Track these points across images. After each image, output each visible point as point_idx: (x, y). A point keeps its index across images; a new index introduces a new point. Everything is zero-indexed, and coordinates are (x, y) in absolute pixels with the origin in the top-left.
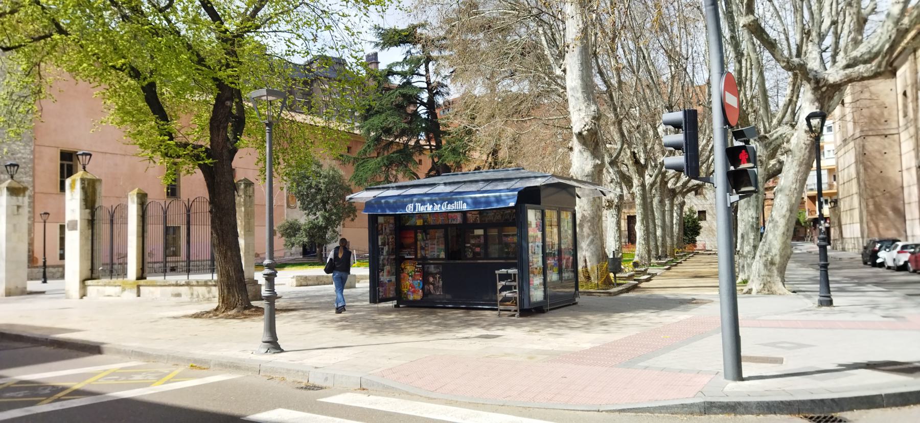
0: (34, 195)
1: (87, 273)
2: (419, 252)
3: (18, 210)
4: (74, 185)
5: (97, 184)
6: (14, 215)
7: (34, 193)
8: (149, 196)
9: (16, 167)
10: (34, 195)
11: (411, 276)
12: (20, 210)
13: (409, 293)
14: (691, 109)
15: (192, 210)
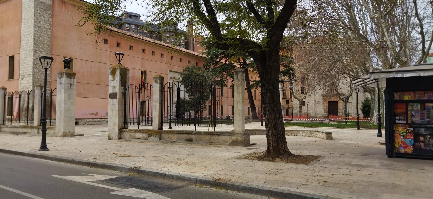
0: (51, 81)
1: (122, 125)
2: (409, 118)
3: (71, 87)
5: (127, 71)
6: (69, 89)
7: (51, 80)
8: (7, 90)
9: (121, 56)
10: (51, 81)
11: (403, 136)
12: (72, 86)
13: (401, 148)
15: (22, 96)
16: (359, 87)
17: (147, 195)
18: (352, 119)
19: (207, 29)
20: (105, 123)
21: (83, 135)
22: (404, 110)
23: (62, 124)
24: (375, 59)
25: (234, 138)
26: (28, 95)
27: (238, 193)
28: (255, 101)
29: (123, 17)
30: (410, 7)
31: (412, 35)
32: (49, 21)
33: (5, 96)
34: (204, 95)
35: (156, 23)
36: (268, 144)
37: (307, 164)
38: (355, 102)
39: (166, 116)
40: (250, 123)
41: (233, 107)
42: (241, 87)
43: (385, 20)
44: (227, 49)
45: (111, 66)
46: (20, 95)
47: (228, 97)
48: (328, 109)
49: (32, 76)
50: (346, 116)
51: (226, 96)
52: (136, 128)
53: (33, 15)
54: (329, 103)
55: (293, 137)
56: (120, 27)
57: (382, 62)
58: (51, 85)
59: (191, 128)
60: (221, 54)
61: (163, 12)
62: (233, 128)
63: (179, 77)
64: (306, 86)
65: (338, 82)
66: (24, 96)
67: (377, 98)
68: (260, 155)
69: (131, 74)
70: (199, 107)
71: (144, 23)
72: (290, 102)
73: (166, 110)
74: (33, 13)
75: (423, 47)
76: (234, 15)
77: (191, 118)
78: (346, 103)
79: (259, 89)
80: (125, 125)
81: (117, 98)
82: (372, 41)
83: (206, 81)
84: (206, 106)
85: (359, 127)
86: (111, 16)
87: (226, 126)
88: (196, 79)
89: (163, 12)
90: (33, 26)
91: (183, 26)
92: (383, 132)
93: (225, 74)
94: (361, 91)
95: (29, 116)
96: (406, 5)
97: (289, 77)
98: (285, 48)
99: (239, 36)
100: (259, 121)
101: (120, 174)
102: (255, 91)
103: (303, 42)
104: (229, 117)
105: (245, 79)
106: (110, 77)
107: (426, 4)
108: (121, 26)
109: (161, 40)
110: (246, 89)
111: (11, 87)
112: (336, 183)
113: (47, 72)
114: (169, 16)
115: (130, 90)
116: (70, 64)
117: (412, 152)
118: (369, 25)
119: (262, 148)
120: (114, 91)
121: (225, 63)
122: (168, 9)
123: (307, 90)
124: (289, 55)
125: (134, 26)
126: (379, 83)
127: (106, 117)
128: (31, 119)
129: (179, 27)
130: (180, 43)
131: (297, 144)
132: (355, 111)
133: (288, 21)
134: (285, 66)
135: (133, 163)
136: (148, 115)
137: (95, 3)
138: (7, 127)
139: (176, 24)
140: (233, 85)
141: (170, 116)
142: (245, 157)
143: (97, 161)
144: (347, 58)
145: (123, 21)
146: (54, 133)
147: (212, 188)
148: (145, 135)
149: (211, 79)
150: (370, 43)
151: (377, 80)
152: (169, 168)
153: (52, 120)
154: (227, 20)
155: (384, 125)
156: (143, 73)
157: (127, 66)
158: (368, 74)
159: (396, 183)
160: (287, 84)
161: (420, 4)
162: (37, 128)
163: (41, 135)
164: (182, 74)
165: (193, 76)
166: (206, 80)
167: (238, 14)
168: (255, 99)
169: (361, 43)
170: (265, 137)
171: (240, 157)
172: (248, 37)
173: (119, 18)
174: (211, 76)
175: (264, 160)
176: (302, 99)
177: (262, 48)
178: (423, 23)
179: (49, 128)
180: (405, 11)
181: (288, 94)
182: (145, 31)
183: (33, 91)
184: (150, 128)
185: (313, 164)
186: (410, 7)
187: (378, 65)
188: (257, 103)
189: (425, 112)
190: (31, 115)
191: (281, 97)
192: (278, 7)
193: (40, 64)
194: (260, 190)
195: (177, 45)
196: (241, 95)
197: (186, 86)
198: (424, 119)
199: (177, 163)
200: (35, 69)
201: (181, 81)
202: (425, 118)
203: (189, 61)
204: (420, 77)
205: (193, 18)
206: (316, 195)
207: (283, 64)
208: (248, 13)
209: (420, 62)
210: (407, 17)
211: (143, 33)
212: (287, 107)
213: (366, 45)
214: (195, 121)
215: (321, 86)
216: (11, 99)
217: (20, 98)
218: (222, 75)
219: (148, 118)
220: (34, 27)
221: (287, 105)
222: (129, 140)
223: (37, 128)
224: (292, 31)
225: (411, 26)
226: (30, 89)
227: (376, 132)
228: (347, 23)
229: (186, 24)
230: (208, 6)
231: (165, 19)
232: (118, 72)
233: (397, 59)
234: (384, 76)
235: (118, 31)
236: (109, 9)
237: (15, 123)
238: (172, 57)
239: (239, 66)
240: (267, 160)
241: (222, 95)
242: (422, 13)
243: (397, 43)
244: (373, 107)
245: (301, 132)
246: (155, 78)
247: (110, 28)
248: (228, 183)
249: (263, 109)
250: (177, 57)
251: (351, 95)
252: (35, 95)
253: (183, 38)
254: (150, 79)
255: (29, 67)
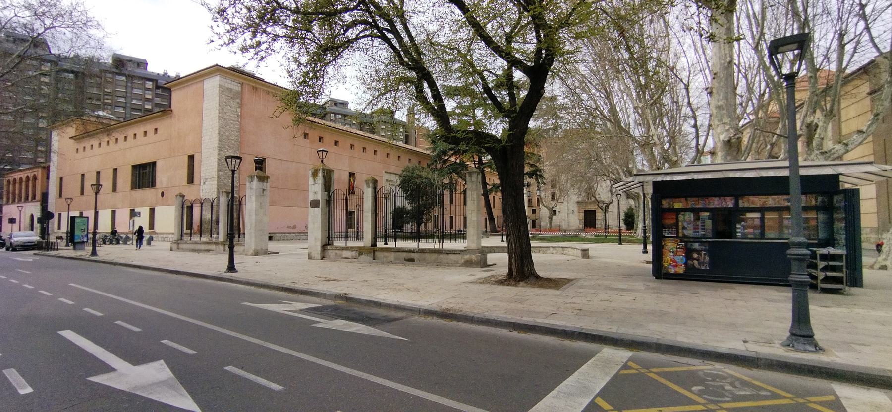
1: (325, 241)
2: (680, 231)
4: (317, 174)
14: (434, 76)
15: (204, 205)
16: (621, 192)
17: (358, 328)
18: (613, 232)
19: (432, 119)
20: (305, 238)
21: (278, 253)
22: (674, 221)
23: (253, 239)
24: (639, 158)
25: (467, 257)
26: (212, 203)
27: (472, 326)
28: (493, 210)
29: (327, 105)
30: (681, 95)
31: (683, 129)
32: (237, 111)
33: (183, 205)
34: (429, 203)
35: (368, 112)
36: (510, 264)
37: (558, 289)
38: (616, 211)
39: (381, 230)
40: (487, 237)
41: (466, 218)
42: (475, 192)
43: (651, 110)
44: (458, 144)
45: (312, 166)
46: (202, 204)
47: (460, 204)
48: (585, 219)
49: (216, 179)
50: (605, 229)
51: (457, 204)
52: (343, 244)
53: (217, 105)
54: (586, 213)
55: (541, 255)
56: (323, 117)
57: (648, 161)
58: (239, 190)
59: (412, 245)
60: (450, 149)
61: (377, 98)
62: (465, 245)
63: (398, 180)
64: (557, 191)
65: (595, 186)
66: (207, 205)
67: (642, 206)
68: (500, 278)
69: (336, 177)
70: (422, 218)
71: (353, 113)
72: (537, 211)
73: (381, 221)
74: (218, 101)
75: (697, 144)
76: (467, 101)
77: (411, 232)
78: (605, 213)
79: (499, 195)
80: (329, 240)
81: (859, 189)
82: (636, 136)
83: (431, 185)
84: (431, 216)
85: (620, 242)
86: (312, 104)
87: (457, 242)
88: (418, 183)
89: (377, 98)
90: (217, 117)
91: (402, 115)
92: (650, 247)
93: (455, 176)
94: (624, 197)
95: (213, 229)
96: (677, 92)
97: (537, 179)
98: (531, 143)
99: (473, 127)
100: (499, 235)
101: (324, 302)
102: (494, 197)
103: (553, 136)
104: (461, 230)
105: (481, 181)
106: (311, 180)
107: (700, 91)
108: (324, 116)
109: (373, 133)
110: (482, 195)
111: (191, 194)
112: (592, 312)
113: (235, 175)
114: (385, 103)
115: (335, 196)
116: (262, 164)
117: (684, 272)
118: (633, 116)
119: (502, 270)
120: (315, 198)
121: (455, 162)
122: (383, 94)
123: (558, 196)
124: (535, 152)
125: (340, 116)
126: (645, 187)
127: (306, 231)
128: (215, 233)
129: (396, 116)
130: (398, 137)
131: (546, 264)
132: (617, 222)
133: (534, 109)
134: (532, 165)
135: (339, 288)
136: (358, 228)
137: (293, 89)
138: (186, 243)
139: (393, 113)
140: (466, 189)
141: (386, 230)
142: (481, 280)
143: (296, 286)
144: (606, 156)
145: (328, 109)
146: (244, 250)
147: (439, 320)
148: (354, 253)
149: (438, 182)
150: (634, 138)
151: (642, 184)
152: (385, 295)
153: (240, 234)
154: (457, 107)
155: (651, 240)
156: (351, 175)
157: (331, 167)
158: (631, 176)
159: (664, 310)
160: (534, 188)
161: (693, 91)
162: (223, 244)
163: (228, 253)
164: (401, 176)
165: (415, 178)
166: (431, 183)
167: (472, 100)
168: (494, 207)
169: (622, 139)
170: (506, 255)
171: (475, 281)
172: (485, 129)
173: (322, 107)
174: (438, 177)
175: (505, 285)
176: (553, 208)
177: (502, 143)
178: (697, 114)
179: (238, 245)
180: (675, 100)
181: (535, 201)
182: (354, 122)
183: (218, 198)
184: (360, 244)
185: (565, 289)
186: (681, 95)
187: (643, 165)
188: (497, 212)
189: (699, 223)
190: (215, 228)
191: (526, 204)
192: (521, 92)
193: (227, 165)
194: (500, 322)
195: (394, 140)
196: (476, 202)
197: (405, 191)
198: (698, 232)
199: (395, 289)
200: (220, 170)
201: (400, 185)
202: (700, 230)
203: (410, 160)
204: (762, 178)
205: (415, 105)
206: (569, 327)
207: (529, 163)
208: (484, 99)
209: (693, 163)
210: (677, 106)
211: (351, 125)
212: (533, 217)
213: (628, 140)
214: (417, 236)
215: (576, 191)
216: (191, 208)
217: (202, 207)
218: (451, 177)
219: (358, 232)
220: (219, 120)
221: (534, 215)
222: (335, 260)
223: (223, 244)
224: (539, 122)
225: (682, 118)
226: (214, 196)
227: (640, 247)
228: (605, 113)
229: (406, 113)
230: (434, 90)
231: (379, 106)
232: (320, 174)
233: (666, 159)
234: (651, 179)
235: (321, 123)
236: (311, 95)
237: (196, 239)
238: (388, 154)
239: (473, 165)
240: (508, 285)
241: (452, 202)
242: (695, 102)
243: (665, 138)
244: (638, 217)
245: (551, 249)
246: (366, 181)
247: (311, 119)
248: (459, 313)
249: (505, 221)
250: (394, 154)
251: (611, 203)
252: (220, 205)
253: (402, 130)
254: (360, 182)
255: (213, 169)
